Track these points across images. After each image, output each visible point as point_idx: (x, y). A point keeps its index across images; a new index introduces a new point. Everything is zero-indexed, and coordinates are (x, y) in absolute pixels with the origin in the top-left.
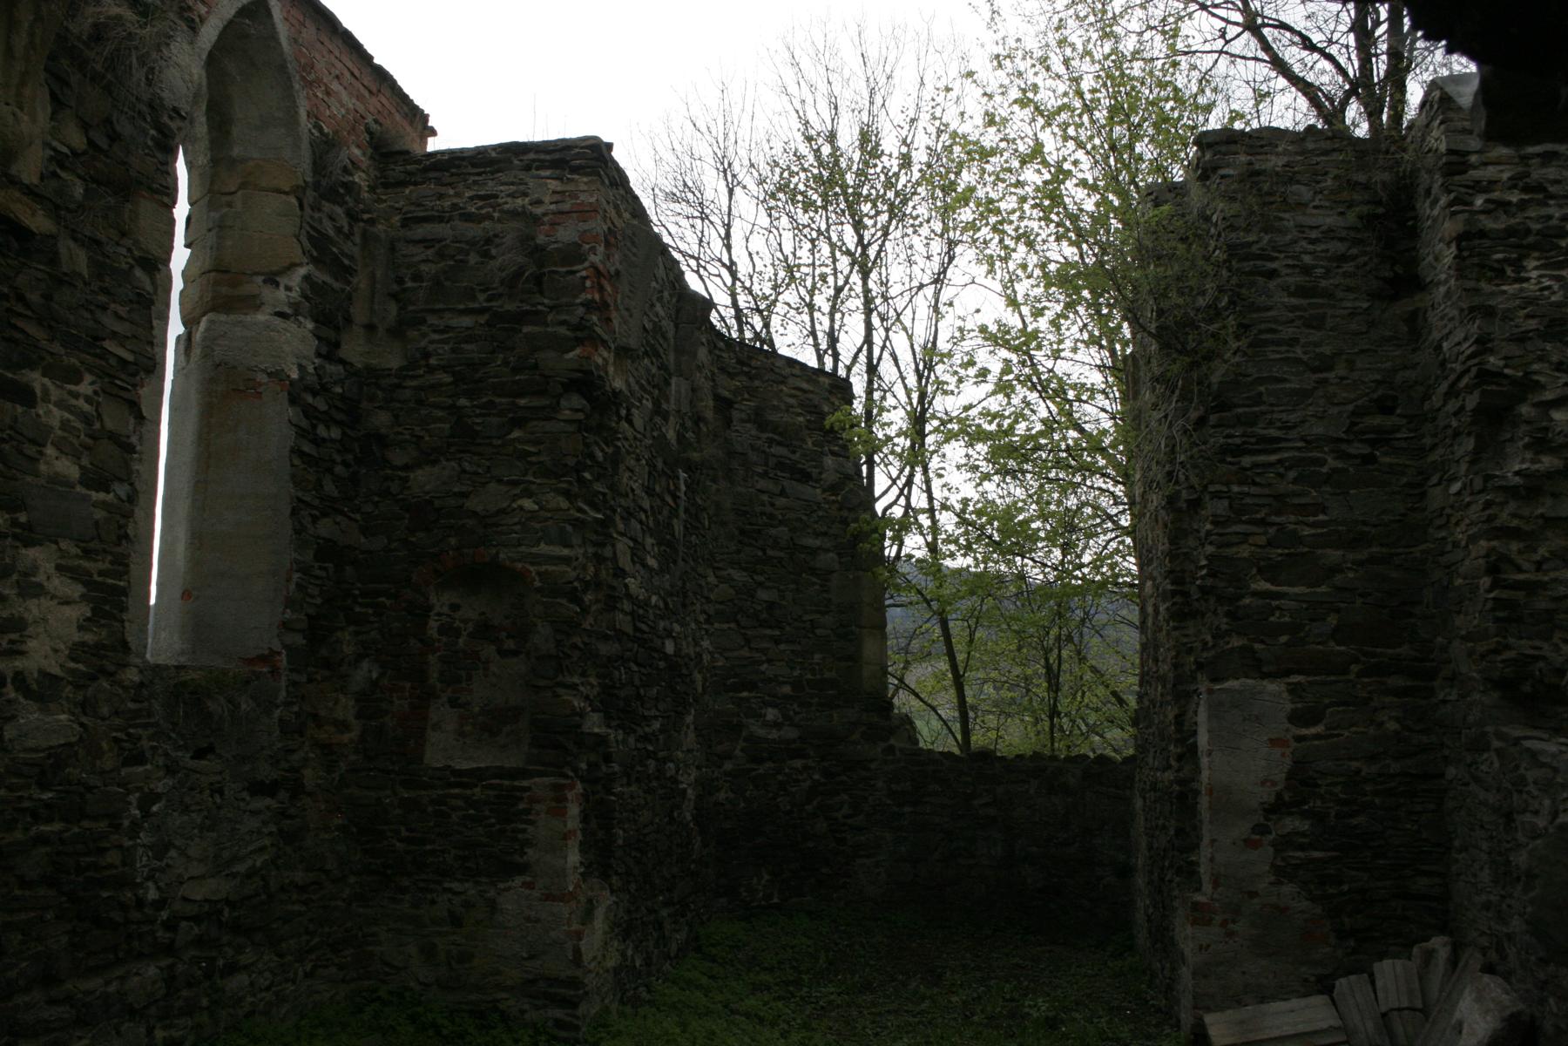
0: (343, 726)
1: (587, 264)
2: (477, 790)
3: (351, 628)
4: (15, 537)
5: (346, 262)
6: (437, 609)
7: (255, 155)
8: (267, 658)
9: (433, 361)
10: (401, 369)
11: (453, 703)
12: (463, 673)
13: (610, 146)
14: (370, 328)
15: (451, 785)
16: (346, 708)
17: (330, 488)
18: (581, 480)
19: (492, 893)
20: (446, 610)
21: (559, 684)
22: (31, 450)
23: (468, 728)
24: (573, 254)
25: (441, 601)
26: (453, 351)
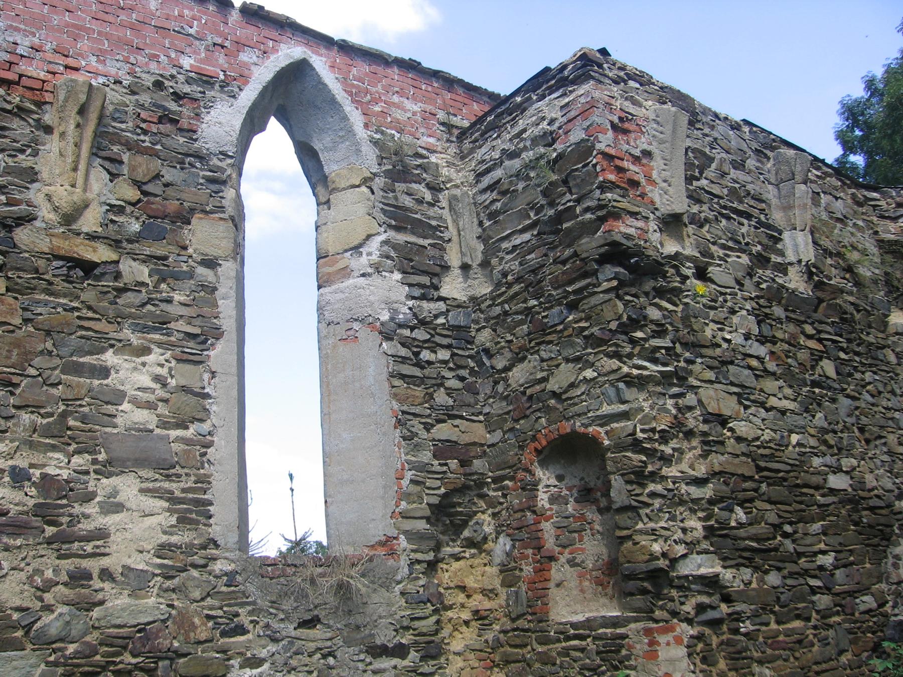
1: (595, 153)
4: (96, 472)
5: (434, 223)
7: (336, 168)
8: (387, 543)
9: (509, 278)
10: (492, 292)
11: (572, 563)
13: (245, 3)
15: (568, 638)
17: (441, 397)
18: (633, 342)
22: (111, 409)
24: (584, 150)
26: (521, 264)
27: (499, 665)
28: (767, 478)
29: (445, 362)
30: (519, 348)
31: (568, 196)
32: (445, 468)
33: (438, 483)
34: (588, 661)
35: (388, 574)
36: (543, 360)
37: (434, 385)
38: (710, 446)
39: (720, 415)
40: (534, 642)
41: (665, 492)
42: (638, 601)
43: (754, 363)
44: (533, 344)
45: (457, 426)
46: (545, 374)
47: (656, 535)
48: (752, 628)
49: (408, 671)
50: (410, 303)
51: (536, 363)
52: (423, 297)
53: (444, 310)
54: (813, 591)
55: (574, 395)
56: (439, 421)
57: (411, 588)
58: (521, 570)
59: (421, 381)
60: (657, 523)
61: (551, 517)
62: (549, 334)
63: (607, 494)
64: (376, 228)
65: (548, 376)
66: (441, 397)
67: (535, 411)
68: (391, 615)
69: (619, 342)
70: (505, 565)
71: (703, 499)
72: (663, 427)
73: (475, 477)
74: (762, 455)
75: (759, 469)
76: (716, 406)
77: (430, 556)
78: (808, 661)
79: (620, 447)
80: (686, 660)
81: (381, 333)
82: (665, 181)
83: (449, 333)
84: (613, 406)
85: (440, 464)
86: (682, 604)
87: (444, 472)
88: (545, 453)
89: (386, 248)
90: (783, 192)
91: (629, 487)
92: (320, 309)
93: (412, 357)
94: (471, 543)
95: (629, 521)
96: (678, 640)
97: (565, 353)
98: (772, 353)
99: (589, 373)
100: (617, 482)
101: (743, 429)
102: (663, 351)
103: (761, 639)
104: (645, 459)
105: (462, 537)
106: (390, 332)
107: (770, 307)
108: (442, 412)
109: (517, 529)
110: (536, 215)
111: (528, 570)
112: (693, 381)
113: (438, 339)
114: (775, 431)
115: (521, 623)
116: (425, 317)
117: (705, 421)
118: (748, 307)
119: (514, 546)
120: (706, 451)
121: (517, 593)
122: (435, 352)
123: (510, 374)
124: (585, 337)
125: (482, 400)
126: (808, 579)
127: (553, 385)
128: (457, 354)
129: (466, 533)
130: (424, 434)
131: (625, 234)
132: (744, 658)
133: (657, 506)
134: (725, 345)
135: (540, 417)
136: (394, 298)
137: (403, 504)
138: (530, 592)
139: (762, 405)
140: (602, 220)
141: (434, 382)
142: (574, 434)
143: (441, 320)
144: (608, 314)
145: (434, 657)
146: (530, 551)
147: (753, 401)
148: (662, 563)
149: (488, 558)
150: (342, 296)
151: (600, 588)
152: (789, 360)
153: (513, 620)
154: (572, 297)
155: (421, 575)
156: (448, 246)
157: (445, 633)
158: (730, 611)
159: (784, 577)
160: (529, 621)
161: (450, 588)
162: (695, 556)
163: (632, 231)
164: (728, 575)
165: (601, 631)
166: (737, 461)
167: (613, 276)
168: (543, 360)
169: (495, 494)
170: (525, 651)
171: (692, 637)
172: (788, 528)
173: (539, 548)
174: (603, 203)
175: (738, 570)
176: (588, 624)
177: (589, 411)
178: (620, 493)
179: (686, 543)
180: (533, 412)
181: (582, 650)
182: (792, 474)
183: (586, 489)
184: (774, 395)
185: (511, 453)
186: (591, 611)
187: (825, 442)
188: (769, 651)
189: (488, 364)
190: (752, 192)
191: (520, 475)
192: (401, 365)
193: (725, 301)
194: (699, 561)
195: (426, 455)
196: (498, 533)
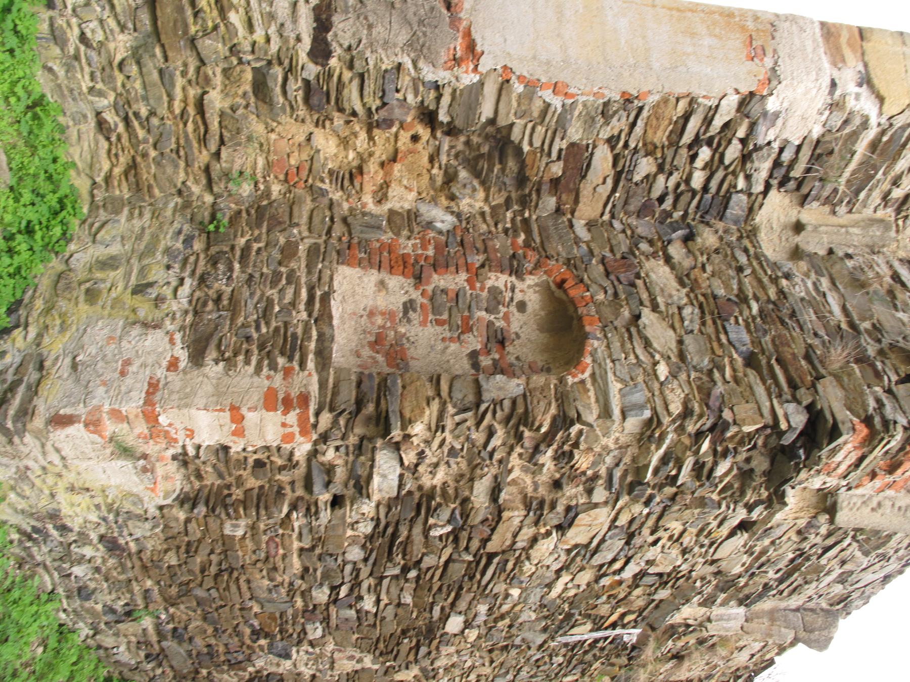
0: (381, 195)
2: (304, 315)
3: (487, 209)
5: (862, 195)
6: (519, 285)
9: (784, 282)
11: (409, 306)
12: (445, 316)
14: (798, 227)
16: (402, 198)
18: (699, 436)
19: (169, 325)
20: (518, 297)
21: (443, 405)
23: (379, 321)
25: (529, 289)
26: (802, 299)
27: (290, 192)
28: (478, 563)
29: (688, 181)
30: (696, 280)
31: (894, 378)
32: (554, 155)
33: (537, 143)
34: (277, 309)
35: (429, 49)
36: (680, 309)
37: (664, 160)
38: (536, 508)
39: (570, 525)
40: (313, 241)
41: (489, 448)
42: (348, 395)
43: (617, 566)
44: (701, 298)
45: (604, 182)
46: (662, 307)
47: (436, 431)
48: (296, 525)
49: (291, 59)
50: (776, 146)
51: (675, 298)
52: (777, 164)
53: (753, 191)
54: (335, 589)
55: (635, 344)
56: (616, 159)
57: (405, 81)
58: (409, 238)
59: (674, 141)
60: (452, 431)
61: (472, 287)
62: (714, 323)
63: (498, 368)
64: (891, 109)
65: (660, 312)
66: (645, 166)
67: (614, 287)
68: (371, 44)
69: (704, 419)
70: (416, 217)
71: (471, 493)
72: (577, 457)
73: (534, 196)
74: (507, 561)
75: (491, 556)
76: (584, 522)
77: (443, 117)
78: (251, 574)
79: (562, 398)
80: (260, 444)
81: (752, 94)
82: (879, 504)
83: (722, 193)
84: (618, 396)
85: (560, 150)
86: (337, 449)
87: (549, 154)
88: (558, 293)
89: (857, 121)
90: (791, 615)
91: (507, 404)
92: (792, 19)
93: (708, 135)
94: (450, 178)
95: (460, 396)
96: (288, 438)
97: (688, 339)
98: (620, 583)
99: (663, 370)
100: (514, 386)
101: (545, 546)
102: (674, 473)
103: (281, 531)
104: (543, 430)
105: (460, 168)
106: (749, 108)
107: (673, 587)
108: (628, 164)
109: (462, 241)
110: (866, 330)
111: (407, 246)
112: (624, 499)
113: (720, 174)
114: (531, 576)
115: (338, 229)
116: (752, 162)
117: (568, 509)
118: (683, 567)
119: (440, 232)
120: (531, 503)
121: (379, 228)
122: (704, 169)
123: (661, 262)
124: (710, 373)
125: (629, 221)
126: (349, 585)
127: (648, 317)
128: (693, 198)
129: (463, 174)
130: (605, 134)
131: (841, 449)
132: (258, 513)
133: (474, 436)
134: (650, 539)
135: (606, 292)
136: (790, 123)
137: (519, 88)
138: (378, 245)
139: (565, 567)
140: (868, 421)
141: (669, 160)
142: (585, 336)
143: (741, 183)
144: (744, 410)
145: (307, 99)
146: (431, 252)
147: (573, 559)
148: (396, 434)
149: (428, 198)
150: (809, 49)
151: (373, 339)
152: (604, 598)
153: (345, 220)
154: (764, 362)
155: (420, 98)
156: (827, 208)
157: (339, 120)
158: (321, 505)
159: (355, 563)
160: (340, 239)
161: (396, 141)
162: (399, 470)
163: (839, 457)
164: (367, 508)
165: (314, 334)
166: (509, 536)
167: (793, 424)
168: (680, 309)
169: (508, 220)
170: (304, 228)
171: (292, 454)
172: (413, 574)
173: (435, 267)
174: (891, 427)
175: (372, 519)
176: (325, 317)
177: (613, 361)
178: (500, 389)
179: (417, 465)
180: (613, 283)
181: (293, 304)
182: (475, 586)
183: (504, 339)
184: (572, 580)
185: (560, 248)
186: (343, 321)
187: (502, 617)
188: (265, 538)
189: (674, 235)
190: (807, 586)
191: (533, 257)
192: (702, 117)
193: (702, 546)
194: (390, 477)
195: (577, 131)
196: (458, 215)
